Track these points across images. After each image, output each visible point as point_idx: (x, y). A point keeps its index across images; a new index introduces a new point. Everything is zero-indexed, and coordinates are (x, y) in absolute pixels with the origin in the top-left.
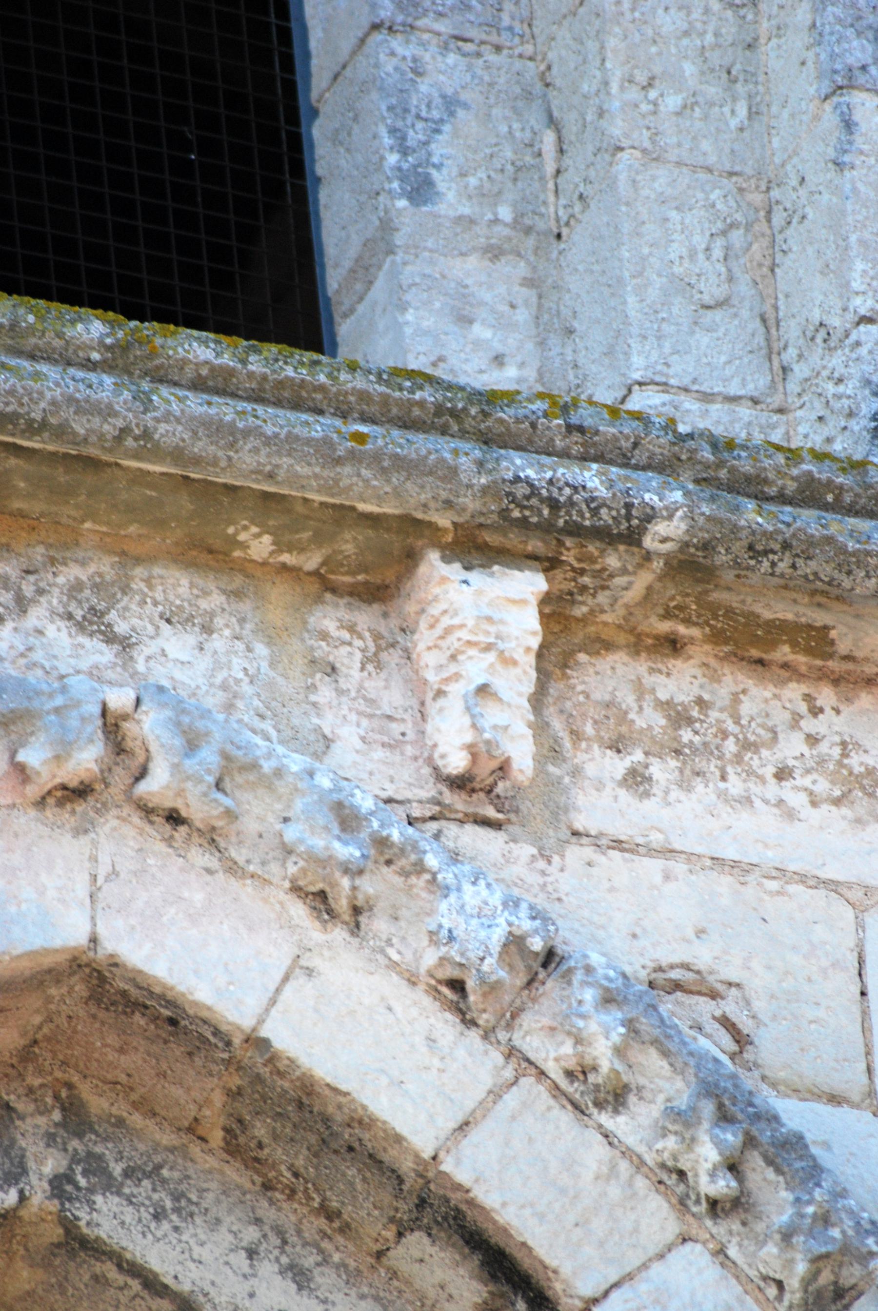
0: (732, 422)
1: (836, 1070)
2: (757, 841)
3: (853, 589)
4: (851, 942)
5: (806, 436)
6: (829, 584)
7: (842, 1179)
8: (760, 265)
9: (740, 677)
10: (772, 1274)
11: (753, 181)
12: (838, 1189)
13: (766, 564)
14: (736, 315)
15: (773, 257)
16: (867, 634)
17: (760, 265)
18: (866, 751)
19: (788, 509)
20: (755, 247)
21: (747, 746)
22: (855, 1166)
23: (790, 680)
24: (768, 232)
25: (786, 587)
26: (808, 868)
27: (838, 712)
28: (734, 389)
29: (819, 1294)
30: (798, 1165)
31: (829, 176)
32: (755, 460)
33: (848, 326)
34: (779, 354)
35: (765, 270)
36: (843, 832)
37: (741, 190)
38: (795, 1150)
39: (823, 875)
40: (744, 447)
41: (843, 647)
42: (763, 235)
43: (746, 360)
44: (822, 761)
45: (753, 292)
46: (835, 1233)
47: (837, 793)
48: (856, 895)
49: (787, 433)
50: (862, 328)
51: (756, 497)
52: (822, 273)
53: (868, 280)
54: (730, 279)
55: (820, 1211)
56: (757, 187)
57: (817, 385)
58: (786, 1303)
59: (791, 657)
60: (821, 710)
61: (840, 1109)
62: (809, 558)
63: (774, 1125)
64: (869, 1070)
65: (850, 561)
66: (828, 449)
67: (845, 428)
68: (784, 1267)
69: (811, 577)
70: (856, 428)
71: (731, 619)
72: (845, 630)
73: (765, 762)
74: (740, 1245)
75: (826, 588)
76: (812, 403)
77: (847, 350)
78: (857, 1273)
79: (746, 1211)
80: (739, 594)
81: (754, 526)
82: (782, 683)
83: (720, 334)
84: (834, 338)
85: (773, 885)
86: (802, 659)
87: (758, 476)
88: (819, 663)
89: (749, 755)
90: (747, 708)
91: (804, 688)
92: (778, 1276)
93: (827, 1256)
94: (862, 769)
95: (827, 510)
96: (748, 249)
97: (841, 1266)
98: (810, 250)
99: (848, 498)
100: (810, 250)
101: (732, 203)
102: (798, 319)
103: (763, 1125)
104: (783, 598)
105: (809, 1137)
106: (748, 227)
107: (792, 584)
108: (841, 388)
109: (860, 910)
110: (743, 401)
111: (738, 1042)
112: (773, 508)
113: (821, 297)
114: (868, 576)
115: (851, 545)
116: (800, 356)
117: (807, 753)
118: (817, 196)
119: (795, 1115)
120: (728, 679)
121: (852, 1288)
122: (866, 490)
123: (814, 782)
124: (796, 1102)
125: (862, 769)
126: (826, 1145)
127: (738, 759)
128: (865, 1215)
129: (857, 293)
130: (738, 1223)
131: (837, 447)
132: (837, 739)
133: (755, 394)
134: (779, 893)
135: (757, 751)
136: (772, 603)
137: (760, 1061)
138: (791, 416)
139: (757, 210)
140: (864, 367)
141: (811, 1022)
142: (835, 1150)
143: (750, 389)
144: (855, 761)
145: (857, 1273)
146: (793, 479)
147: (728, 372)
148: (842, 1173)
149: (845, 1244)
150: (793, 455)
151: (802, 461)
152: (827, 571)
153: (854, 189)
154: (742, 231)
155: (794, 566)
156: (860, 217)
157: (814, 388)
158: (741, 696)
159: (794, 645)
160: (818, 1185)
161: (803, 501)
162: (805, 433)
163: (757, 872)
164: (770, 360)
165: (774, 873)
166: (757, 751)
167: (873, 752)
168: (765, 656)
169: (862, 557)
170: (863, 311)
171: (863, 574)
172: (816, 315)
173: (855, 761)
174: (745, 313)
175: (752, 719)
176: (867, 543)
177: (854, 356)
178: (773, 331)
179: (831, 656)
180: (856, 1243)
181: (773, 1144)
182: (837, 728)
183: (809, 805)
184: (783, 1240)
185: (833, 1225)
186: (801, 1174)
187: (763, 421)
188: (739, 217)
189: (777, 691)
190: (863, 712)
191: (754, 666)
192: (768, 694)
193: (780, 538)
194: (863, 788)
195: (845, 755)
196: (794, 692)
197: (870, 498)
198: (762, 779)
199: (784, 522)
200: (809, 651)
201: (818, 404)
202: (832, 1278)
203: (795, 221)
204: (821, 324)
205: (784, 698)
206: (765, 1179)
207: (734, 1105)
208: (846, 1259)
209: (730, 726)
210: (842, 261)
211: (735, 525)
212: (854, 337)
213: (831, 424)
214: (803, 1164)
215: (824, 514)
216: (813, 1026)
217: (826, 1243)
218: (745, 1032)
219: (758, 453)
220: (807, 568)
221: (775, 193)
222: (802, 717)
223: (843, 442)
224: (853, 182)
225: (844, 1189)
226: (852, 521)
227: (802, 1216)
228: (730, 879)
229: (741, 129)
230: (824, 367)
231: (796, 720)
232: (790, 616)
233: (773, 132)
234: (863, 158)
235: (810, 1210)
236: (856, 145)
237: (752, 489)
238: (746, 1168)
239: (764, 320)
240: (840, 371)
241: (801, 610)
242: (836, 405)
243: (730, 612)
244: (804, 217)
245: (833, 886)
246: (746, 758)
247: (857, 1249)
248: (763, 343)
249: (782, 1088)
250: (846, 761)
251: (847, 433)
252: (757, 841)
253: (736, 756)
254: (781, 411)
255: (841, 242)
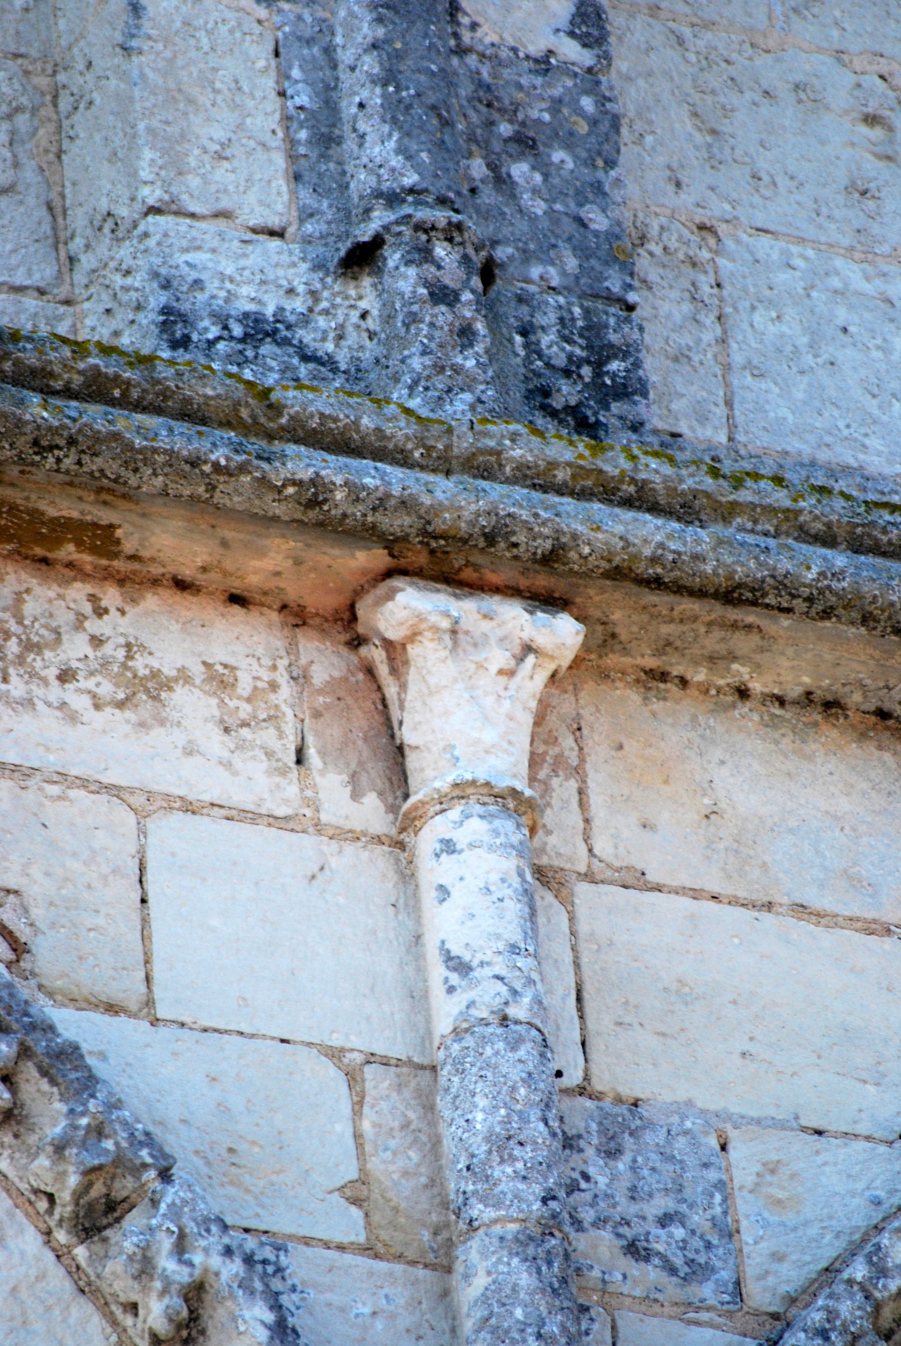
0: (17, 313)
1: (114, 979)
2: (39, 744)
3: (139, 487)
4: (132, 848)
5: (93, 329)
6: (116, 481)
7: (117, 1089)
8: (47, 151)
9: (24, 576)
10: (43, 1187)
11: (39, 65)
12: (113, 1100)
13: (51, 460)
14: (21, 202)
15: (60, 142)
16: (153, 534)
17: (47, 151)
18: (150, 654)
19: (74, 403)
20: (41, 132)
21: (30, 647)
22: (130, 1077)
23: (75, 579)
24: (55, 117)
25: (71, 484)
26: (90, 772)
27: (123, 612)
28: (19, 279)
29: (91, 1207)
30: (73, 1075)
31: (116, 60)
32: (41, 353)
33: (136, 216)
34: (66, 243)
35: (51, 156)
36: (126, 736)
37: (26, 73)
38: (71, 1061)
39: (105, 780)
40: (29, 339)
41: (129, 547)
42: (49, 120)
43: (32, 249)
44: (105, 664)
45: (39, 178)
46: (109, 1144)
47: (121, 696)
48: (138, 800)
49: (74, 325)
50: (150, 218)
51: (42, 391)
52: (110, 161)
53: (156, 169)
54: (16, 165)
55: (93, 1123)
56: (44, 70)
57: (104, 276)
58: (57, 1216)
59: (76, 556)
60: (106, 611)
61: (117, 1019)
62: (95, 454)
63: (50, 1035)
64: (148, 979)
65: (136, 460)
66: (115, 342)
67: (133, 322)
68: (56, 1180)
69: (97, 474)
70: (144, 322)
71: (15, 516)
72: (131, 529)
73: (48, 664)
74: (12, 1158)
75: (112, 485)
76: (99, 294)
77: (135, 241)
78: (130, 1186)
79: (19, 1123)
80: (23, 490)
81: (39, 421)
82: (66, 582)
83: (6, 222)
84: (122, 228)
85: (53, 790)
86: (87, 558)
87: (43, 369)
88: (104, 562)
89: (32, 656)
90: (30, 608)
91: (89, 588)
92: (49, 1189)
93: (100, 1168)
94: (147, 672)
95: (114, 406)
96: (34, 134)
97: (113, 1178)
98: (97, 137)
99: (135, 394)
100: (97, 137)
101: (17, 86)
102: (85, 208)
103: (38, 1035)
104: (69, 496)
105: (85, 1047)
106: (34, 111)
107: (77, 480)
108: (129, 281)
109: (142, 815)
110: (29, 292)
111: (15, 950)
112: (59, 402)
113: (109, 186)
114: (155, 474)
115: (138, 442)
116: (88, 246)
117: (91, 655)
118: (104, 82)
119: (71, 1024)
120: (11, 578)
121: (124, 1200)
122: (153, 385)
123: (98, 684)
124: (73, 1011)
125: (147, 672)
126: (102, 1056)
127: (20, 660)
128: (140, 1126)
129: (145, 183)
130: (10, 1135)
131: (125, 341)
132: (122, 640)
133: (42, 284)
134: (59, 798)
135: (39, 653)
136: (57, 500)
137: (37, 970)
138: (78, 308)
139: (43, 94)
140: (152, 259)
141: (90, 930)
142: (111, 1061)
143: (36, 279)
144: (140, 664)
145: (130, 1186)
146: (79, 372)
147: (14, 260)
148: (118, 1084)
149: (118, 1156)
150: (80, 348)
151: (89, 354)
152: (113, 468)
153: (142, 76)
154: (27, 116)
155: (79, 463)
156: (148, 104)
157: (101, 280)
158: (25, 596)
159: (79, 544)
160: (93, 1096)
161: (89, 395)
162: (92, 326)
163: (38, 776)
164: (57, 250)
165: (56, 778)
166: (39, 653)
167: (158, 654)
168: (49, 555)
169: (149, 454)
170: (151, 201)
171: (150, 472)
172: (104, 204)
173: (140, 664)
174: (31, 201)
175: (36, 619)
176: (153, 440)
177: (142, 247)
178: (60, 220)
179: (116, 555)
180: (129, 1155)
181: (48, 1054)
182: (121, 630)
183: (92, 709)
184: (55, 1152)
185: (107, 1137)
186: (76, 1085)
187: (49, 313)
188: (24, 100)
189: (61, 591)
190: (148, 613)
191: (38, 565)
192: (52, 594)
193: (65, 433)
194: (147, 691)
195: (129, 657)
196: (78, 592)
197: (157, 394)
198: (45, 681)
199: (69, 417)
200: (93, 550)
201: (105, 296)
202: (104, 1190)
203: (82, 106)
204: (109, 214)
205: (68, 598)
206: (39, 1091)
207: (9, 1014)
208: (119, 1171)
209: (13, 626)
210: (130, 149)
211: (20, 420)
212: (141, 228)
213: (119, 317)
214: (79, 1075)
215: (110, 409)
216: (92, 934)
217: (99, 1155)
218: (23, 940)
219: (43, 345)
220: (93, 465)
221: (61, 77)
222: (86, 618)
223: (130, 335)
224: (140, 68)
225: (119, 1100)
226: (139, 417)
227: (76, 1128)
228: (10, 783)
229: (27, 10)
230: (112, 259)
231: (80, 621)
232: (75, 514)
233: (59, 13)
234: (151, 43)
235: (84, 1121)
236: (144, 30)
237: (37, 383)
238: (20, 1079)
239: (50, 208)
240: (128, 262)
241: (88, 508)
242: (124, 297)
243: (13, 509)
244: (91, 103)
245: (114, 791)
246: (29, 660)
247: (130, 1160)
248: (49, 232)
249: (59, 997)
250: (130, 664)
251: (135, 327)
252: (39, 744)
253: (18, 657)
254: (68, 302)
255: (128, 130)
